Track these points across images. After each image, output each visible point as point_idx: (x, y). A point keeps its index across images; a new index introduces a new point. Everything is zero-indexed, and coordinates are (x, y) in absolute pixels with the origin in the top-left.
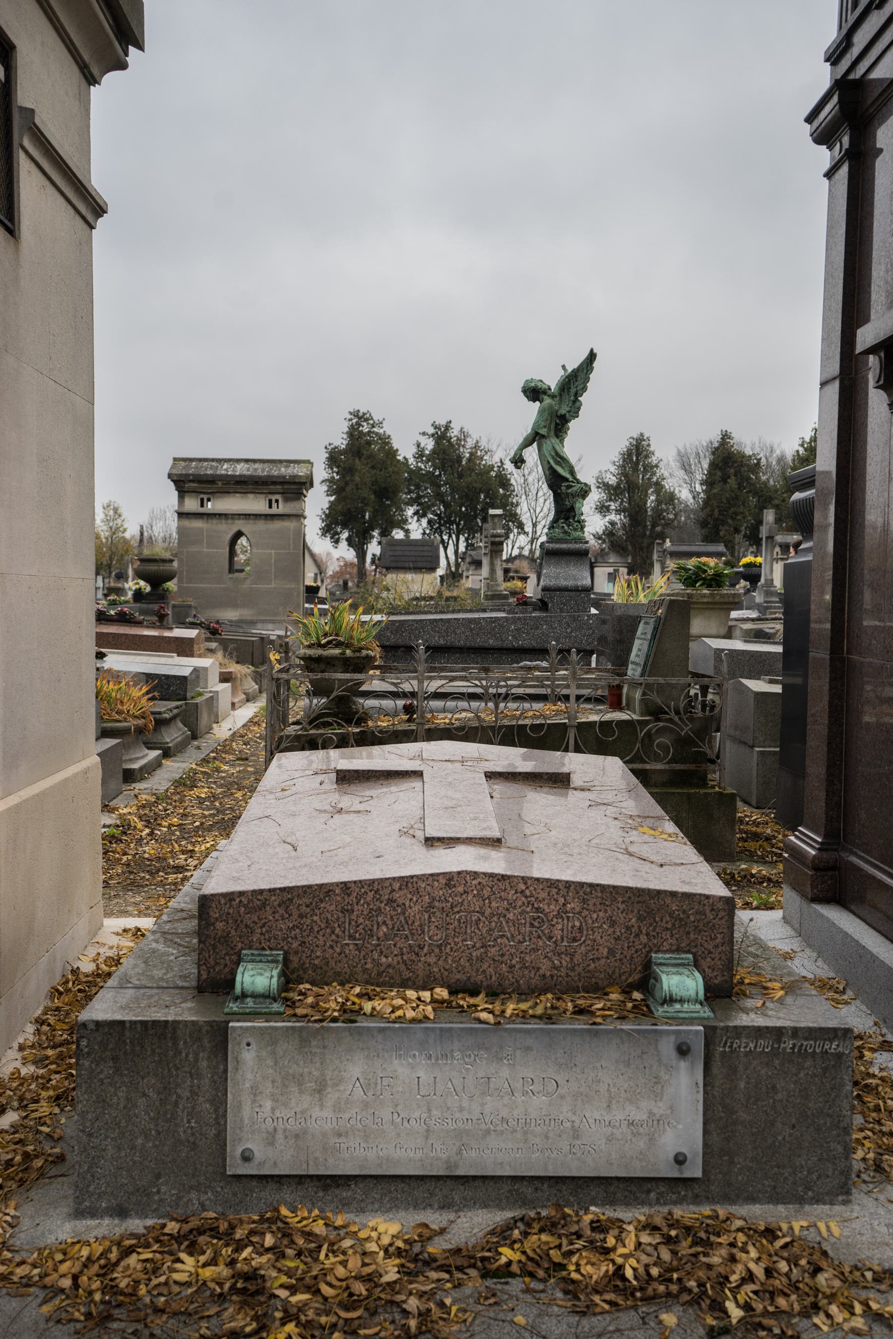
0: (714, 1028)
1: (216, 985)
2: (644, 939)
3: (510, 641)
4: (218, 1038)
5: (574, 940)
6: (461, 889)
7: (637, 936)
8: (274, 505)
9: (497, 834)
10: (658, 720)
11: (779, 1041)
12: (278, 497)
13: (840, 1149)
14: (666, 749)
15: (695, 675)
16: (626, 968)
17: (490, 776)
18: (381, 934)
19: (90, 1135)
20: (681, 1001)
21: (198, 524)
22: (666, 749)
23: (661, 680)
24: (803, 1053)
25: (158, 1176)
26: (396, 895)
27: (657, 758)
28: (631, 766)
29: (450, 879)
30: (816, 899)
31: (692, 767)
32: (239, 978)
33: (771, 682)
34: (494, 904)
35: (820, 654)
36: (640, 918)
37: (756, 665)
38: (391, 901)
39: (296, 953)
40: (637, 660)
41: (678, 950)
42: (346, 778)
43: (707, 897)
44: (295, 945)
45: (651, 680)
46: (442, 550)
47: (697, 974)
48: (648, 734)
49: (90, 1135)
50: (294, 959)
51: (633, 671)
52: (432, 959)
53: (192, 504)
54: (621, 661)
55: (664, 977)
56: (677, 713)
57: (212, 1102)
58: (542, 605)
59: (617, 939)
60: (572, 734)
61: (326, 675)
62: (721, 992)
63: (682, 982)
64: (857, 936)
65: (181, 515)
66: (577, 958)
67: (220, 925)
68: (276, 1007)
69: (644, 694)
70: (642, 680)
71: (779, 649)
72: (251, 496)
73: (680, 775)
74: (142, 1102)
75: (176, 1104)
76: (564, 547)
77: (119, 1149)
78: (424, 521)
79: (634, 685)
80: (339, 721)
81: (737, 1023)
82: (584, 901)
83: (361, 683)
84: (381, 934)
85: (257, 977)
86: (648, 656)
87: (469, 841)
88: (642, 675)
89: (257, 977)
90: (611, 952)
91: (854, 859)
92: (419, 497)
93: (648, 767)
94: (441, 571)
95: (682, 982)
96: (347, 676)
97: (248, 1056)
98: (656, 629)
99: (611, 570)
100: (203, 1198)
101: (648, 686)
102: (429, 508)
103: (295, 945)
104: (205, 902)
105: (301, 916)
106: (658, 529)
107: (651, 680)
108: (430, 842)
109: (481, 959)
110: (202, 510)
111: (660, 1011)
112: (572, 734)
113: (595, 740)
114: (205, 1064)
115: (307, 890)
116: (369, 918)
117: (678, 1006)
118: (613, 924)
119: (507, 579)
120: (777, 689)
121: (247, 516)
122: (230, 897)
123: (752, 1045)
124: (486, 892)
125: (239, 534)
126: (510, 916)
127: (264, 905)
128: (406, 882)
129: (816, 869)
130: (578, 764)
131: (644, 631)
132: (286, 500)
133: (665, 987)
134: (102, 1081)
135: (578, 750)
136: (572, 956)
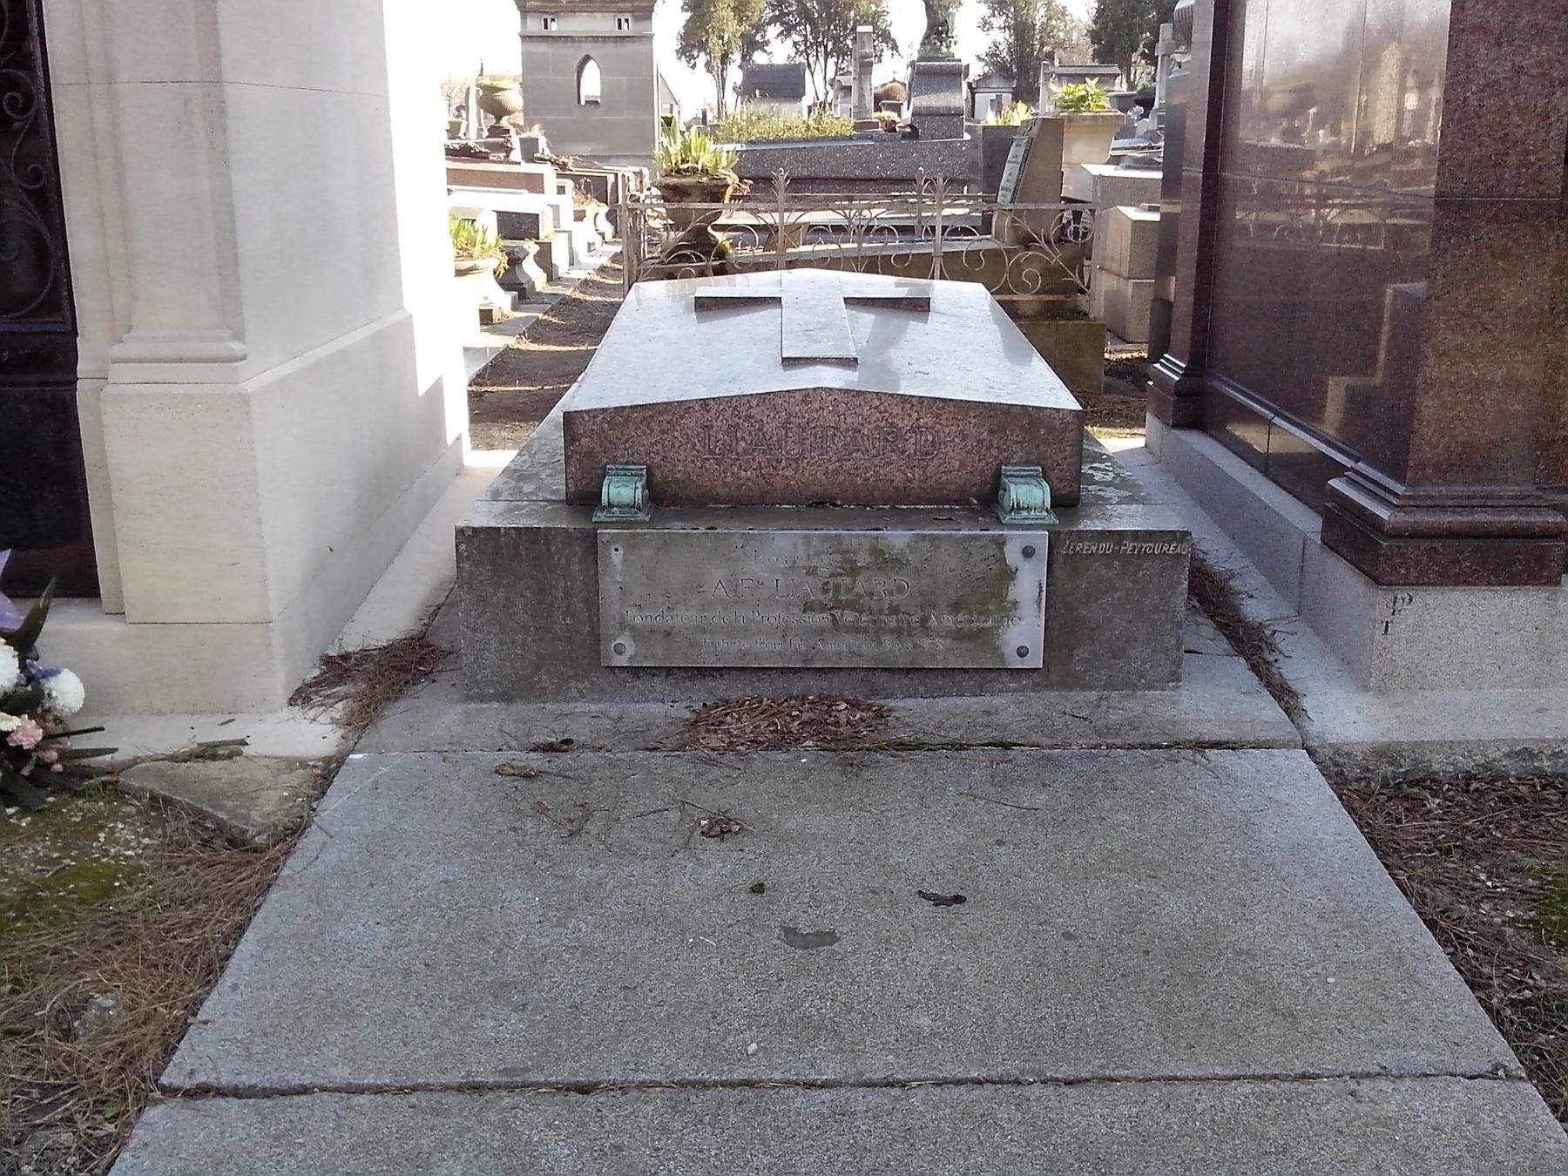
0: (1059, 533)
1: (584, 499)
2: (994, 452)
3: (877, 171)
4: (591, 544)
5: (927, 454)
6: (817, 405)
7: (988, 449)
8: (624, 25)
9: (854, 354)
10: (1028, 248)
11: (1120, 544)
12: (628, 16)
13: (1173, 641)
14: (1034, 279)
15: (1069, 200)
16: (978, 480)
17: (851, 302)
18: (740, 449)
19: (475, 630)
20: (1028, 509)
21: (542, 48)
22: (1034, 279)
23: (1032, 207)
24: (1142, 556)
25: (538, 668)
26: (753, 412)
27: (1025, 290)
28: (1002, 297)
29: (806, 395)
30: (1174, 426)
31: (1061, 297)
32: (604, 490)
33: (1151, 209)
34: (849, 420)
35: (1194, 171)
36: (991, 432)
37: (1134, 192)
38: (749, 417)
39: (659, 467)
40: (1007, 185)
41: (1028, 463)
42: (706, 306)
43: (1057, 410)
44: (658, 459)
45: (1020, 206)
46: (808, 73)
47: (1045, 483)
48: (1017, 263)
49: (475, 630)
50: (658, 474)
51: (1003, 197)
52: (789, 473)
53: (535, 26)
54: (992, 186)
55: (1012, 487)
56: (1048, 242)
57: (585, 602)
58: (913, 133)
59: (969, 452)
60: (937, 264)
61: (683, 205)
62: (1066, 503)
63: (1030, 494)
64: (1213, 458)
65: (525, 38)
66: (930, 471)
67: (584, 441)
68: (641, 516)
69: (1014, 221)
70: (1011, 206)
71: (1159, 175)
72: (598, 15)
73: (1050, 314)
74: (519, 601)
75: (552, 604)
76: (935, 70)
77: (502, 644)
78: (789, 42)
79: (1004, 212)
80: (697, 252)
81: (1081, 527)
82: (938, 416)
83: (718, 215)
84: (740, 449)
85: (621, 490)
86: (1018, 180)
87: (825, 361)
88: (1012, 201)
89: (621, 490)
90: (963, 464)
91: (1217, 384)
92: (782, 14)
93: (1015, 298)
94: (808, 100)
95: (1030, 494)
96: (705, 205)
97: (617, 557)
98: (1027, 151)
99: (993, 96)
100: (581, 686)
101: (1019, 213)
102: (794, 27)
103: (658, 459)
104: (569, 417)
105: (663, 432)
106: (1047, 49)
107: (1020, 206)
108: (790, 362)
109: (836, 472)
110: (545, 33)
111: (1007, 519)
112: (937, 264)
113: (957, 268)
114: (577, 567)
115: (667, 406)
116: (727, 433)
117: (1025, 513)
118: (964, 438)
119: (878, 109)
120: (1156, 217)
121: (595, 39)
122: (593, 413)
123: (1094, 548)
124: (842, 407)
125: (587, 59)
126: (865, 431)
127: (626, 421)
128: (763, 398)
129: (1178, 394)
130: (942, 291)
131: (1016, 152)
132: (637, 19)
133: (1013, 496)
134: (481, 582)
135: (942, 277)
136: (925, 468)
